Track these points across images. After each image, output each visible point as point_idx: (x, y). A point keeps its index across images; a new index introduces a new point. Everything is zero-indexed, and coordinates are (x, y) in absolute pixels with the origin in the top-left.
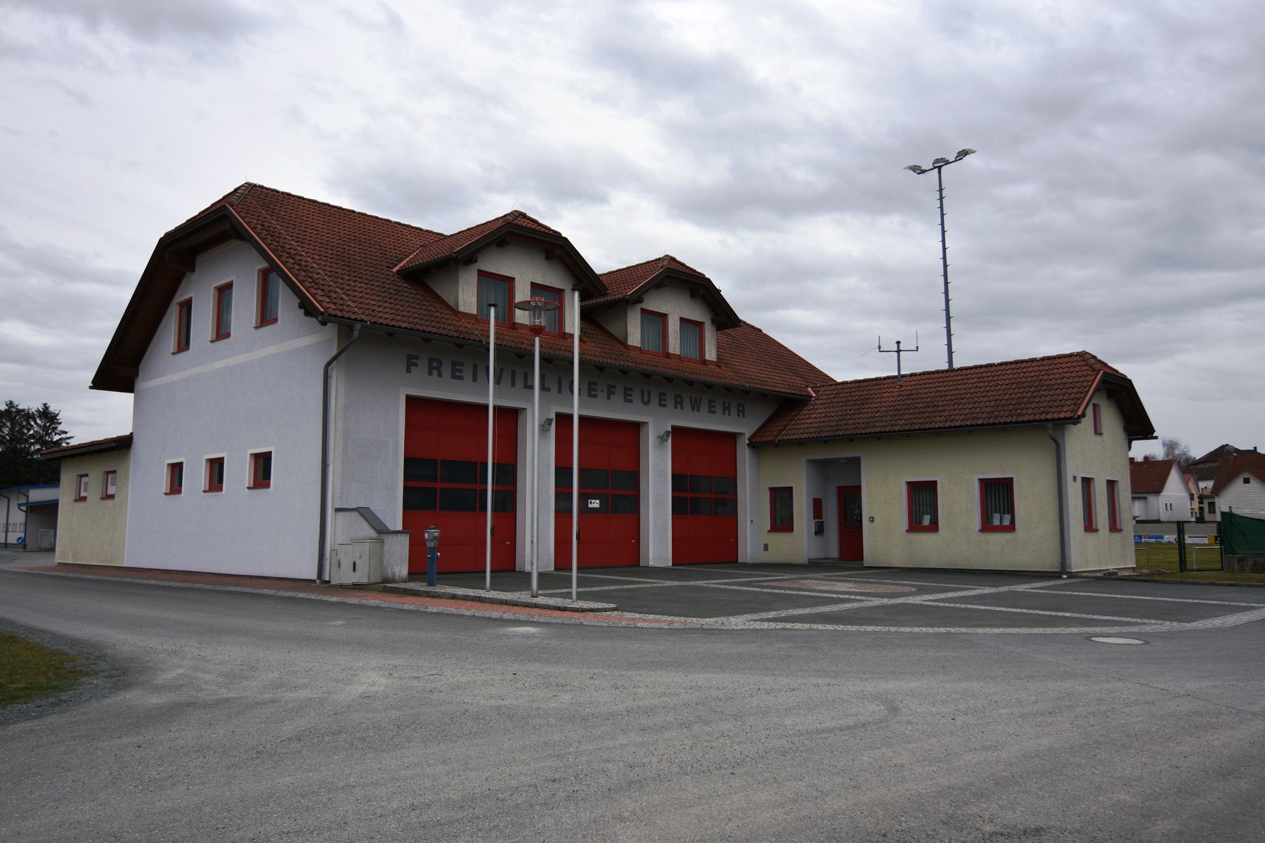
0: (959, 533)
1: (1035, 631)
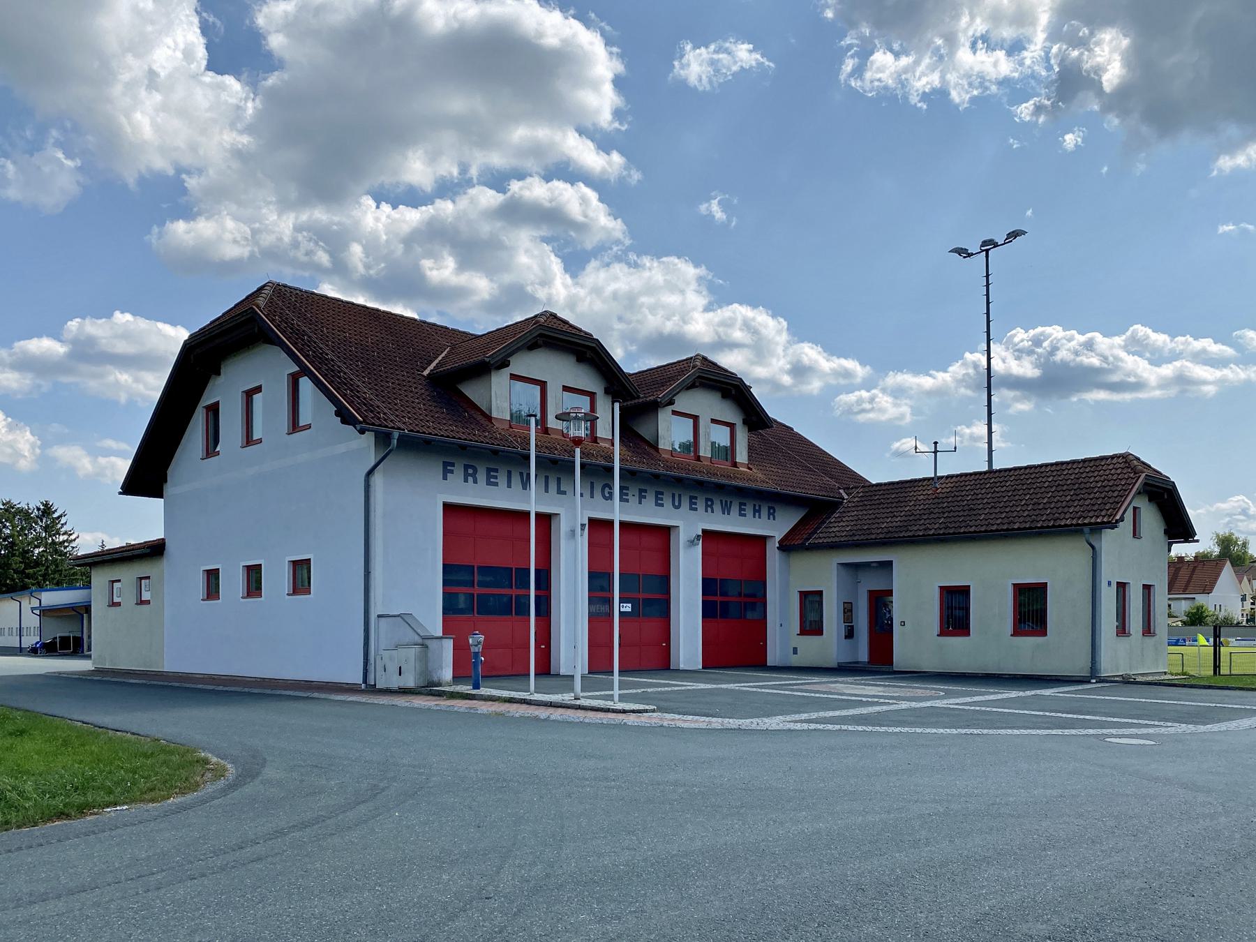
0: (992, 636)
1: (1054, 732)
